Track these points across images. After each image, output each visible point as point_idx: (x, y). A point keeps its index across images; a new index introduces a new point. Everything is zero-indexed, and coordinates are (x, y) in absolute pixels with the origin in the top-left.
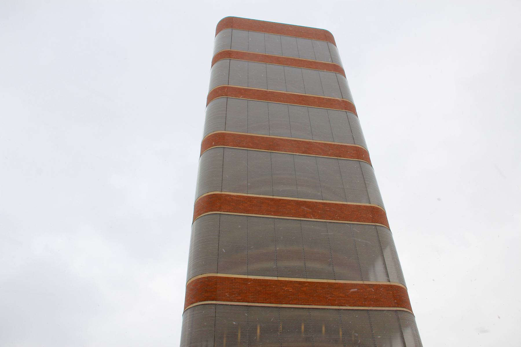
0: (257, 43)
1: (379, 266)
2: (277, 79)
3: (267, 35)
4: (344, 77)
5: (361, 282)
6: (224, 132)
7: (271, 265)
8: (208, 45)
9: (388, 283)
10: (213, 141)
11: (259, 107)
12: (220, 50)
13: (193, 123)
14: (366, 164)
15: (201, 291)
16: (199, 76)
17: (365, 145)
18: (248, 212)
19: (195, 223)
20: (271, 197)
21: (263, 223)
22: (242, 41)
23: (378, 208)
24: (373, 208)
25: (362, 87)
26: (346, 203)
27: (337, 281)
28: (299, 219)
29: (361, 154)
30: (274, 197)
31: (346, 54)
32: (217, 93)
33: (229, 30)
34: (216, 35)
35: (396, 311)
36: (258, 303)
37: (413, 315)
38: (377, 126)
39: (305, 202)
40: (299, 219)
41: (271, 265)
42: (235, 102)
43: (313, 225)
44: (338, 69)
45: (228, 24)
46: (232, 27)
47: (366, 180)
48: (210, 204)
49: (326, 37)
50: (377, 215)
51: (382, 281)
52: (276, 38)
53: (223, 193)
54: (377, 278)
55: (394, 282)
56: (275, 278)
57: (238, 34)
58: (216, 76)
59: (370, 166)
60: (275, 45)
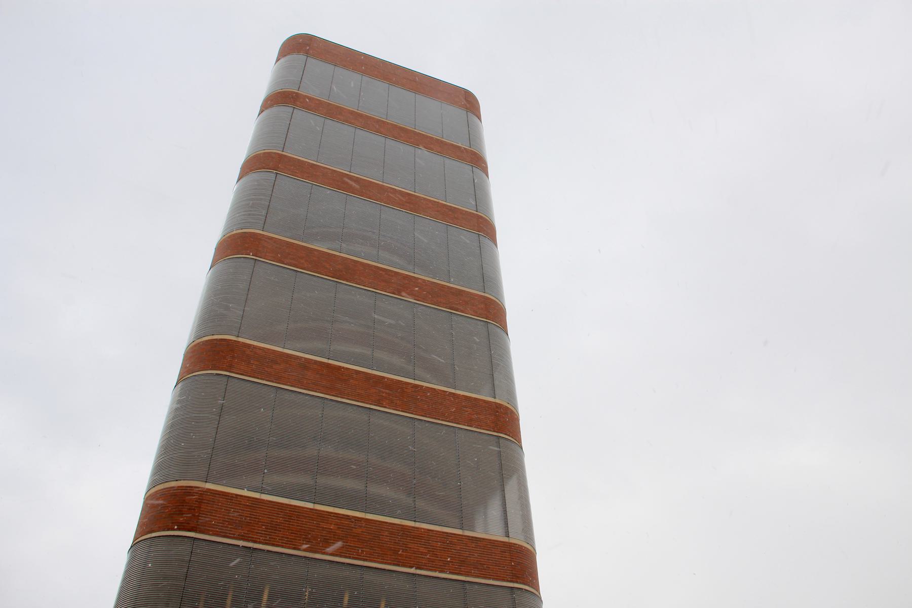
0: (347, 89)
1: (494, 511)
2: (369, 158)
3: (365, 79)
4: (484, 175)
5: (459, 532)
6: (261, 232)
7: (303, 479)
8: (261, 74)
9: (506, 539)
10: (238, 246)
11: (330, 201)
12: (278, 89)
13: (209, 205)
14: (499, 330)
15: (172, 511)
16: (235, 128)
17: (502, 297)
18: (278, 380)
19: (179, 385)
20: (325, 360)
21: (308, 404)
22: (319, 80)
23: (507, 408)
24: (499, 406)
25: (513, 196)
26: (453, 391)
27: (417, 525)
28: (368, 406)
29: (491, 312)
30: (330, 362)
31: (496, 137)
32: (261, 162)
33: (302, 57)
34: (278, 60)
35: (512, 588)
36: (273, 545)
37: (540, 598)
38: (527, 267)
39: (340, 368)
40: (368, 406)
41: (303, 479)
42: (288, 184)
43: (388, 420)
44: (477, 161)
45: (301, 46)
46: (307, 53)
47: (494, 361)
48: (212, 356)
49: (467, 102)
50: (502, 421)
51: (495, 533)
52: (380, 87)
53: (240, 340)
54: (489, 527)
55: (516, 538)
56: (310, 505)
57: (317, 67)
58: (265, 132)
59: (505, 335)
60: (378, 99)
